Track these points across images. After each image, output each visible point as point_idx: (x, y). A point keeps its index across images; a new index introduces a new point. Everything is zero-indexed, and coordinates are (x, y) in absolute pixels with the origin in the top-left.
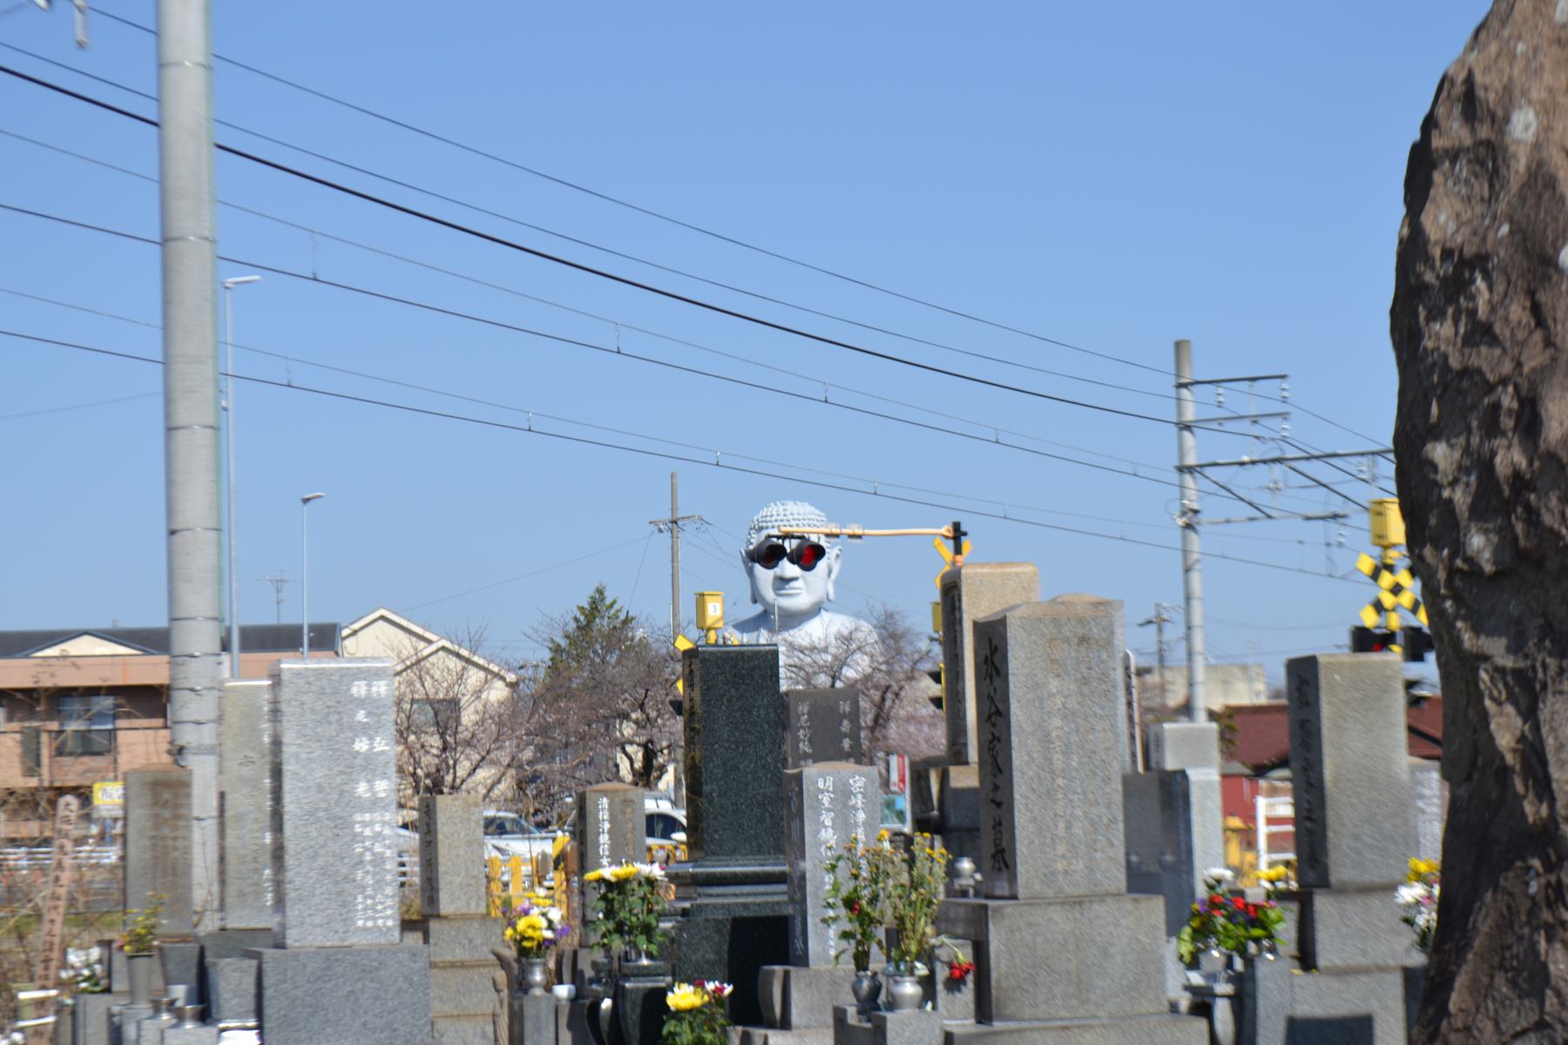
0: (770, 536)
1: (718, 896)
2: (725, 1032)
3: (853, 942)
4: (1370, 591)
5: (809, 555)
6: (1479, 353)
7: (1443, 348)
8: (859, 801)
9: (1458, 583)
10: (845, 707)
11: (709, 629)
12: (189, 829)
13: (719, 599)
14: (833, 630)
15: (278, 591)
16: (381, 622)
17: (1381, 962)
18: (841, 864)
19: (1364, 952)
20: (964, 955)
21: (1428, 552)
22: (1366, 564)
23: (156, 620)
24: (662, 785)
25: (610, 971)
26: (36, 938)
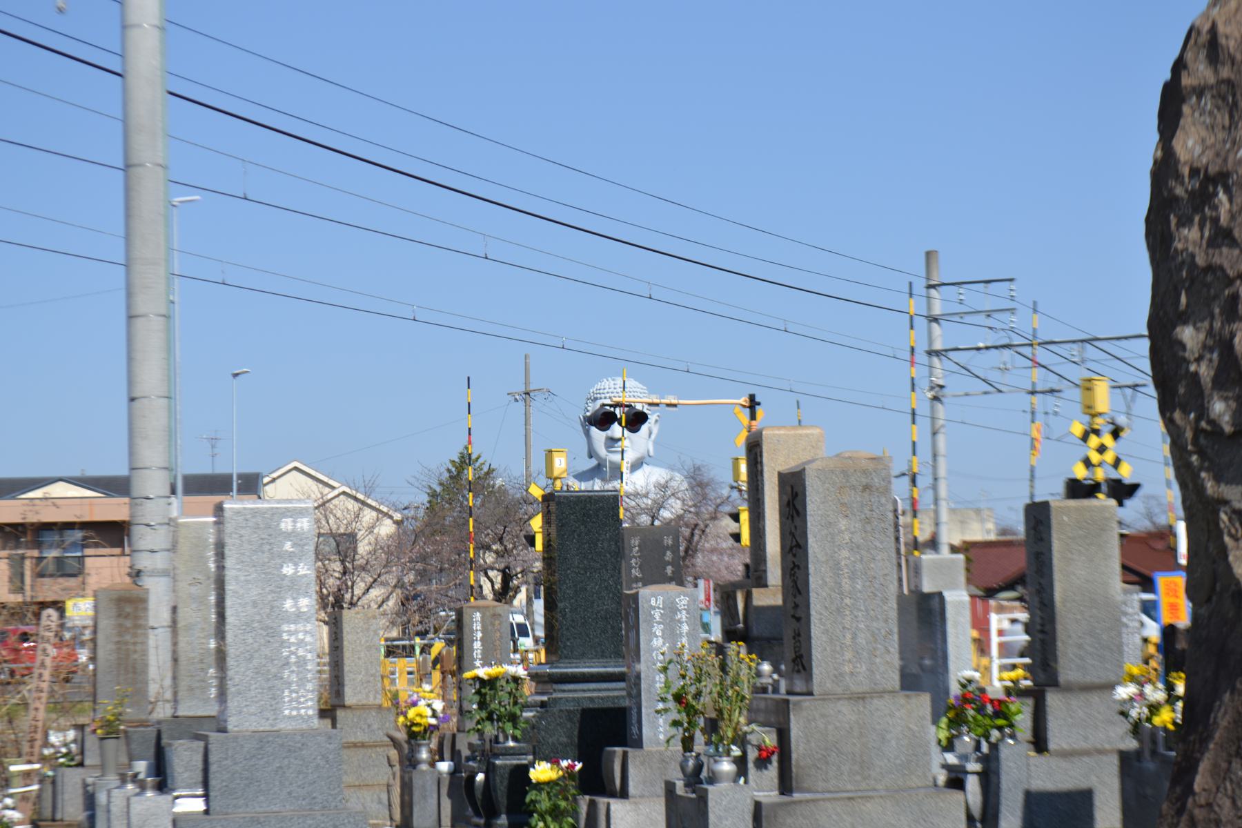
1: (570, 691)
2: (575, 800)
3: (681, 729)
4: (1081, 451)
6: (1221, 254)
7: (1191, 249)
8: (683, 616)
9: (1202, 441)
10: (668, 541)
11: (556, 479)
12: (146, 636)
14: (653, 479)
15: (213, 447)
16: (294, 472)
17: (1099, 746)
18: (670, 666)
19: (1086, 738)
20: (770, 740)
21: (1177, 415)
22: (1077, 429)
23: (119, 469)
24: (516, 602)
25: (483, 751)
26: (24, 722)
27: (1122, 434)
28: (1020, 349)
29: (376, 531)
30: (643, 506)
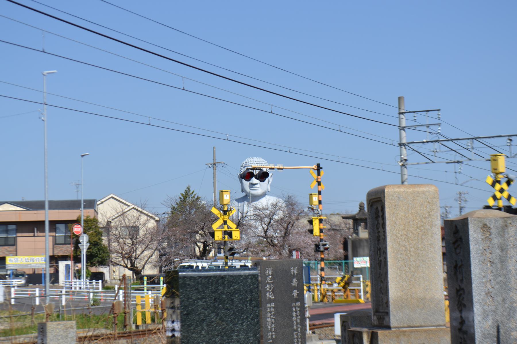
0: (248, 169)
5: (263, 176)
10: (294, 271)
13: (229, 193)
14: (270, 202)
15: (77, 188)
16: (111, 199)
22: (490, 180)
27: (512, 183)
28: (443, 143)
29: (146, 225)
30: (266, 214)
